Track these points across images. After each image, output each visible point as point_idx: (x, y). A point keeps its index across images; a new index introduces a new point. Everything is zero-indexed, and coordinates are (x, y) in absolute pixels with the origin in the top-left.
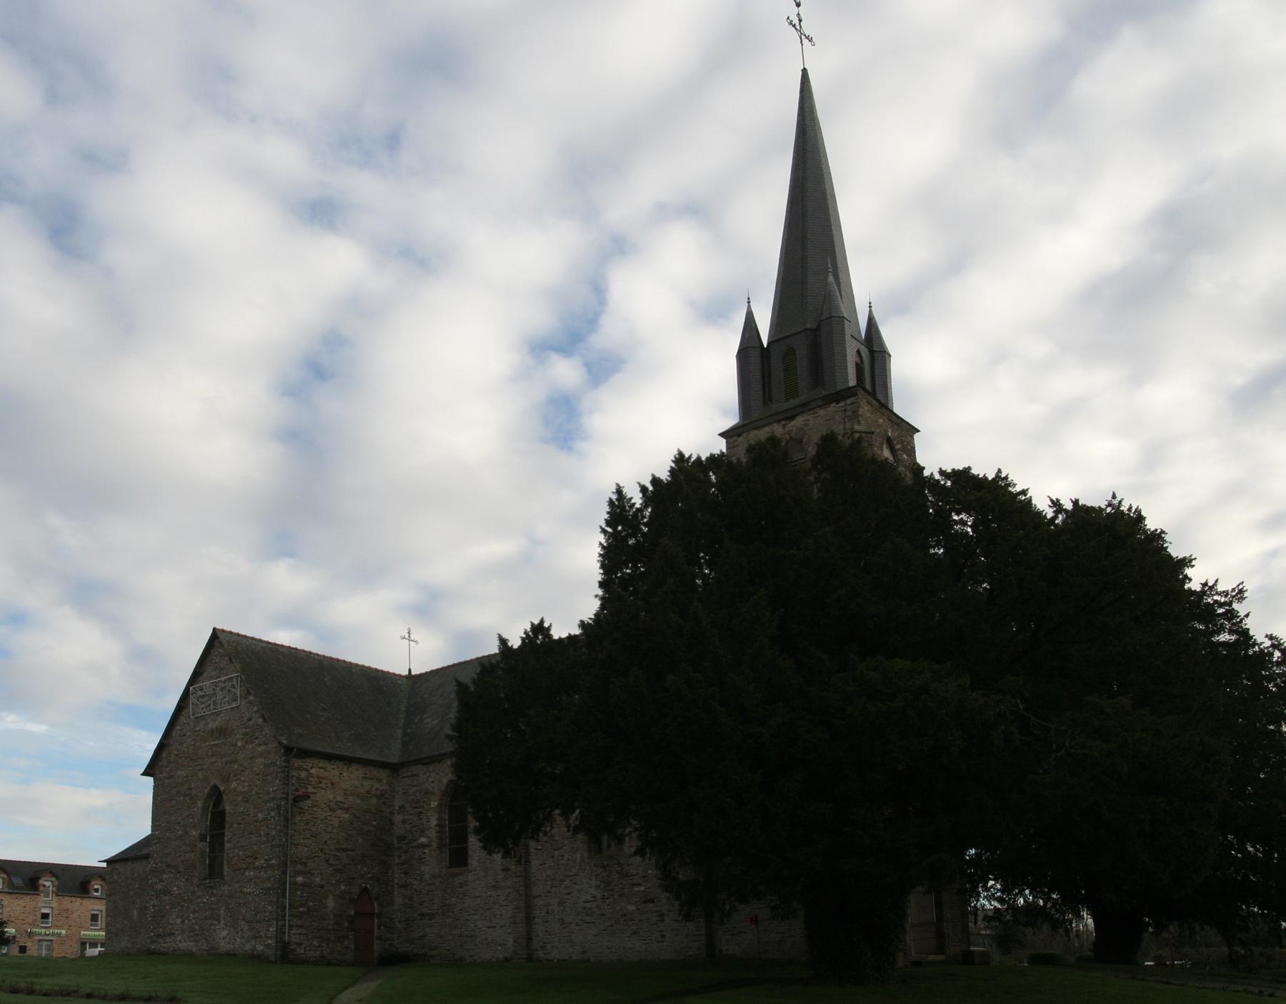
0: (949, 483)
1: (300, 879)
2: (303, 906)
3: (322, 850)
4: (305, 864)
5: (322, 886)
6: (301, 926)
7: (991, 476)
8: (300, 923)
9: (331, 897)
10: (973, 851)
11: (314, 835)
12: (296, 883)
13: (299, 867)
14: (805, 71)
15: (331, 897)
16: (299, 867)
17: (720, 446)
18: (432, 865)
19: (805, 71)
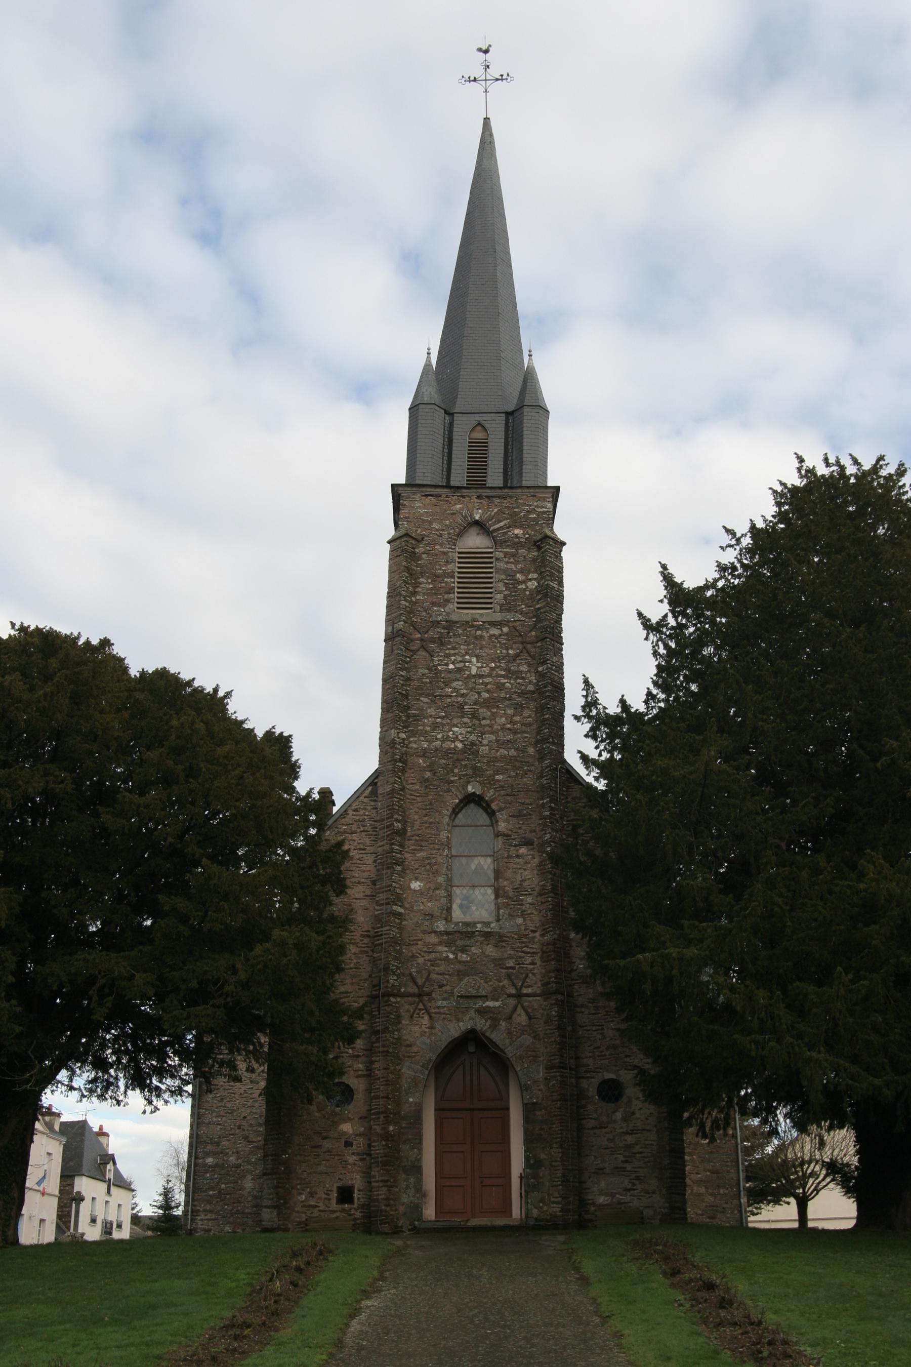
0: (718, 619)
1: (210, 1160)
2: (212, 1189)
3: (239, 1128)
4: (218, 1144)
5: (238, 1166)
6: (211, 1211)
7: (209, 689)
8: (208, 1207)
9: (249, 1177)
10: (851, 509)
11: (232, 1112)
12: (205, 1165)
13: (209, 1147)
14: (487, 120)
15: (249, 1177)
16: (209, 1147)
17: (260, 733)
18: (351, 1152)
19: (487, 120)
